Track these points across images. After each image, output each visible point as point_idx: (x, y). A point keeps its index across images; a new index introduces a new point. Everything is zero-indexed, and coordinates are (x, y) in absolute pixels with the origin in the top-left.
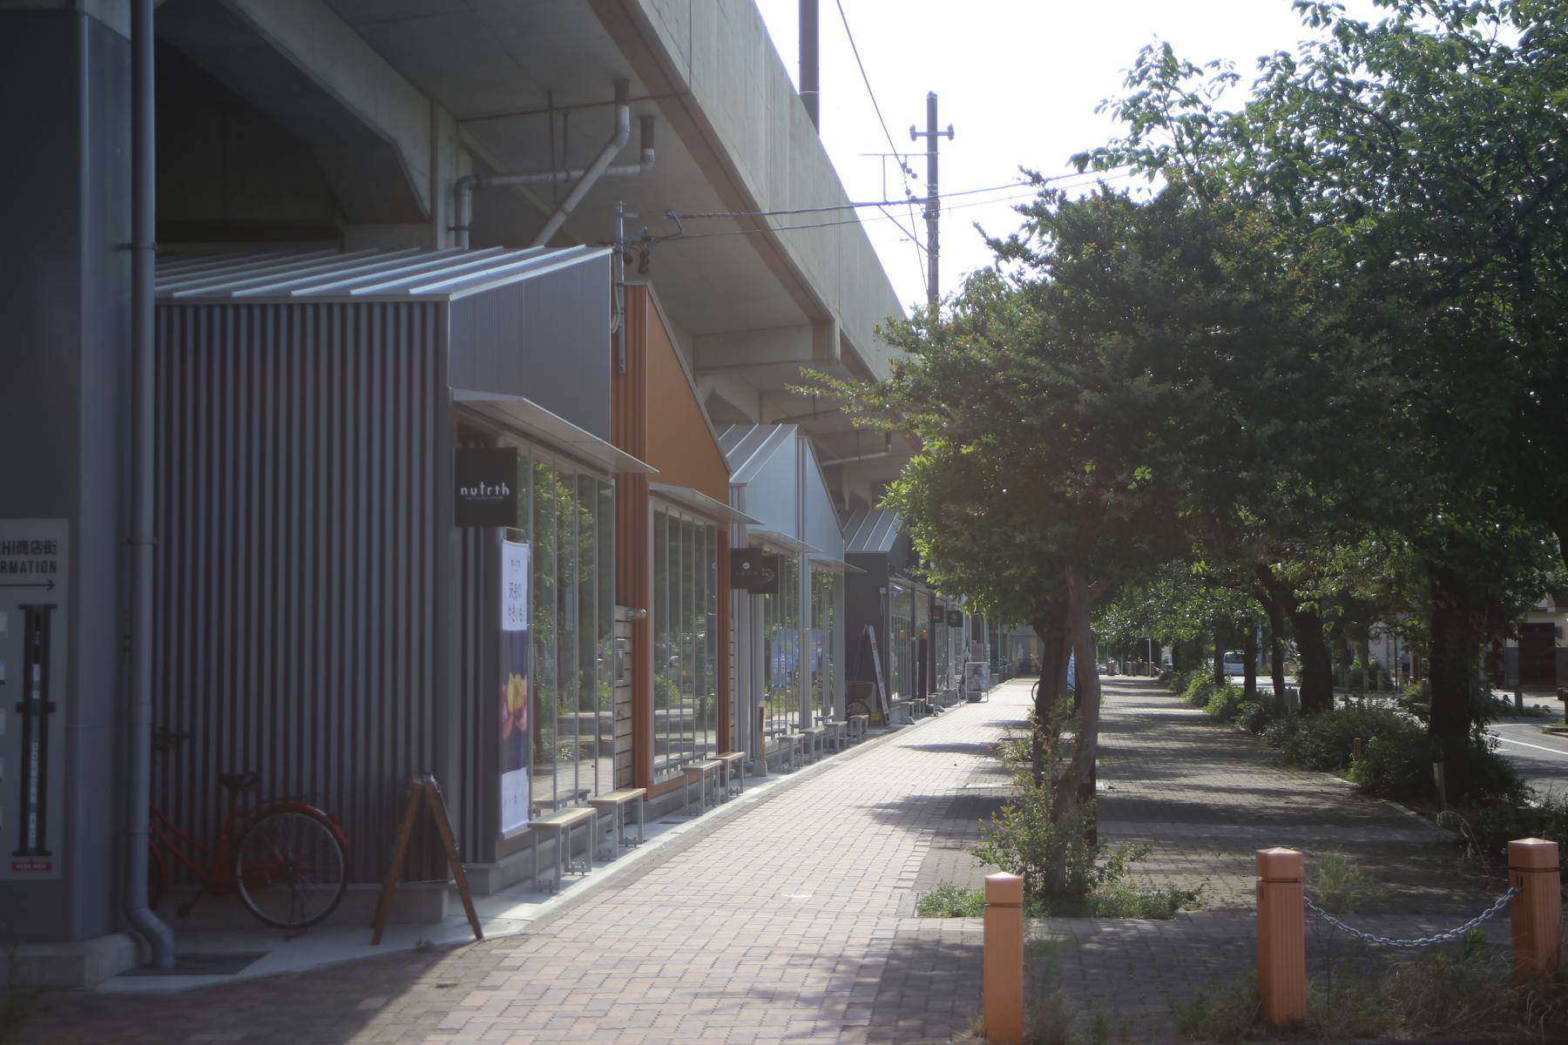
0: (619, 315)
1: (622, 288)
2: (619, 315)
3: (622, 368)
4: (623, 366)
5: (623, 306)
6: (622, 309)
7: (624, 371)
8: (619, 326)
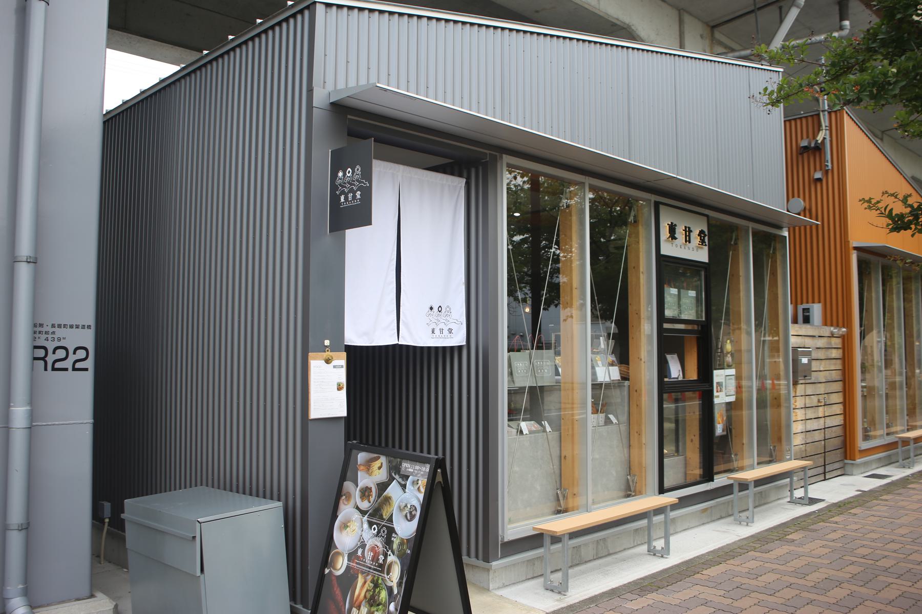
0: (824, 131)
1: (826, 113)
2: (824, 131)
3: (827, 166)
4: (829, 164)
5: (827, 124)
6: (826, 126)
7: (830, 167)
8: (824, 138)
